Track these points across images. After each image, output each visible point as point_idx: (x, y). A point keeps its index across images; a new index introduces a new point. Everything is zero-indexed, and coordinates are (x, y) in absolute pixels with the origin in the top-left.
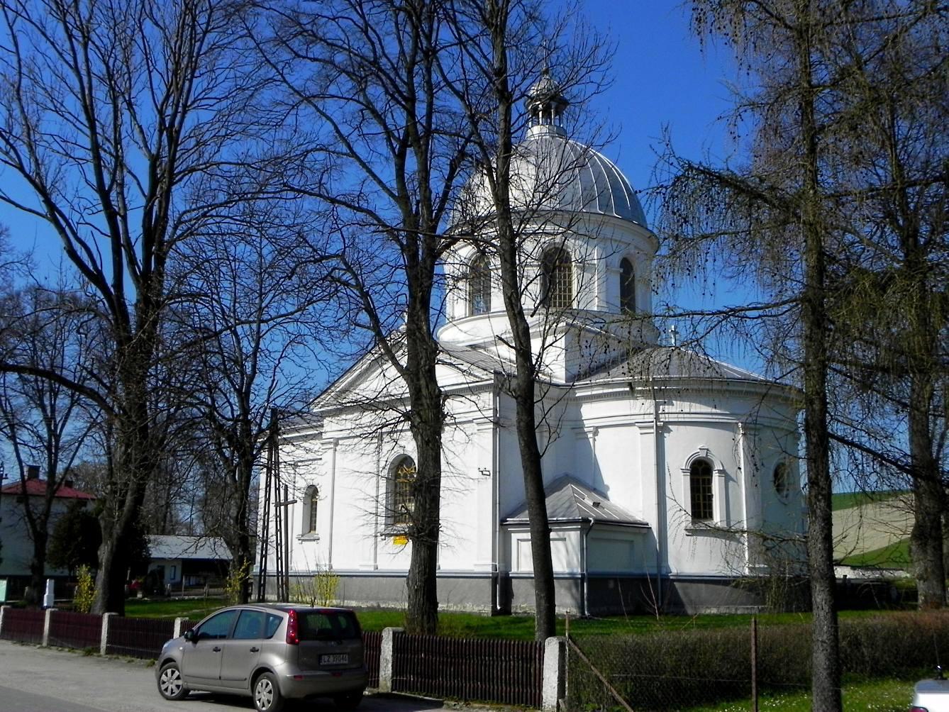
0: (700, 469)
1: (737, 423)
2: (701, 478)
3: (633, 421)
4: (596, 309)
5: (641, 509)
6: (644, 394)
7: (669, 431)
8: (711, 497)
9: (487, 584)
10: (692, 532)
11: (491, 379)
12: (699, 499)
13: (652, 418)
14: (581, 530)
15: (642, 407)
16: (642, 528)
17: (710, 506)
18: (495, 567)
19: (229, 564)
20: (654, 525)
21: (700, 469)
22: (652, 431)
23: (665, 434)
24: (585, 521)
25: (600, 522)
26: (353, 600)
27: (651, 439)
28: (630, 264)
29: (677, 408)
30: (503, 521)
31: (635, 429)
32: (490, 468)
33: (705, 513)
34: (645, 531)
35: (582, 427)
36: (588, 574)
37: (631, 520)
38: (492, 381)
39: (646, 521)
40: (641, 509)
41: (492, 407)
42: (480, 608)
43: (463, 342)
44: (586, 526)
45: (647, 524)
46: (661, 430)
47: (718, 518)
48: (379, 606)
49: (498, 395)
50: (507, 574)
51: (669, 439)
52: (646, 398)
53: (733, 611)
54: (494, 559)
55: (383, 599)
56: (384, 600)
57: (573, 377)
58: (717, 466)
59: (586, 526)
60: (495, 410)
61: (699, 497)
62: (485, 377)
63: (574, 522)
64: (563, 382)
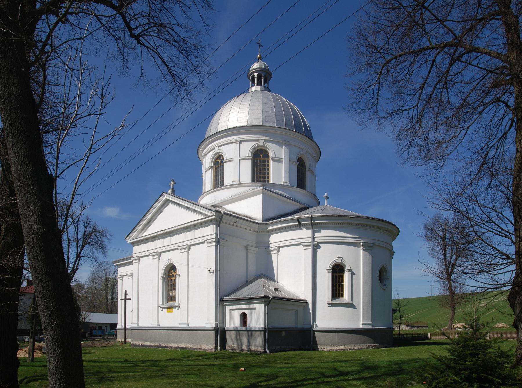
0: (338, 269)
1: (360, 243)
2: (338, 275)
3: (299, 242)
4: (283, 184)
5: (303, 293)
6: (306, 226)
7: (320, 247)
8: (343, 286)
9: (213, 333)
10: (331, 305)
11: (213, 215)
12: (336, 287)
13: (311, 240)
14: (264, 303)
15: (306, 234)
16: (304, 303)
17: (343, 291)
18: (216, 324)
19: (246, 326)
20: (310, 301)
21: (338, 269)
22: (310, 247)
23: (317, 249)
24: (267, 297)
25: (276, 298)
26: (148, 342)
27: (310, 252)
28: (303, 161)
29: (325, 234)
30: (221, 300)
31: (301, 247)
32: (214, 268)
33: (339, 294)
34: (305, 304)
35: (269, 247)
36: (269, 328)
37: (297, 298)
38: (214, 217)
39: (306, 299)
40: (303, 293)
41: (215, 232)
42: (209, 347)
43: (209, 204)
44: (267, 300)
45: (306, 301)
46: (316, 247)
47: (346, 297)
48: (160, 345)
49: (219, 226)
50: (224, 328)
51: (319, 252)
52: (307, 229)
53: (352, 348)
54: (216, 320)
55: (162, 342)
56: (163, 342)
57: (267, 219)
58: (347, 268)
59: (267, 300)
60: (217, 234)
61: (336, 285)
62: (211, 215)
63: (260, 298)
64: (261, 222)
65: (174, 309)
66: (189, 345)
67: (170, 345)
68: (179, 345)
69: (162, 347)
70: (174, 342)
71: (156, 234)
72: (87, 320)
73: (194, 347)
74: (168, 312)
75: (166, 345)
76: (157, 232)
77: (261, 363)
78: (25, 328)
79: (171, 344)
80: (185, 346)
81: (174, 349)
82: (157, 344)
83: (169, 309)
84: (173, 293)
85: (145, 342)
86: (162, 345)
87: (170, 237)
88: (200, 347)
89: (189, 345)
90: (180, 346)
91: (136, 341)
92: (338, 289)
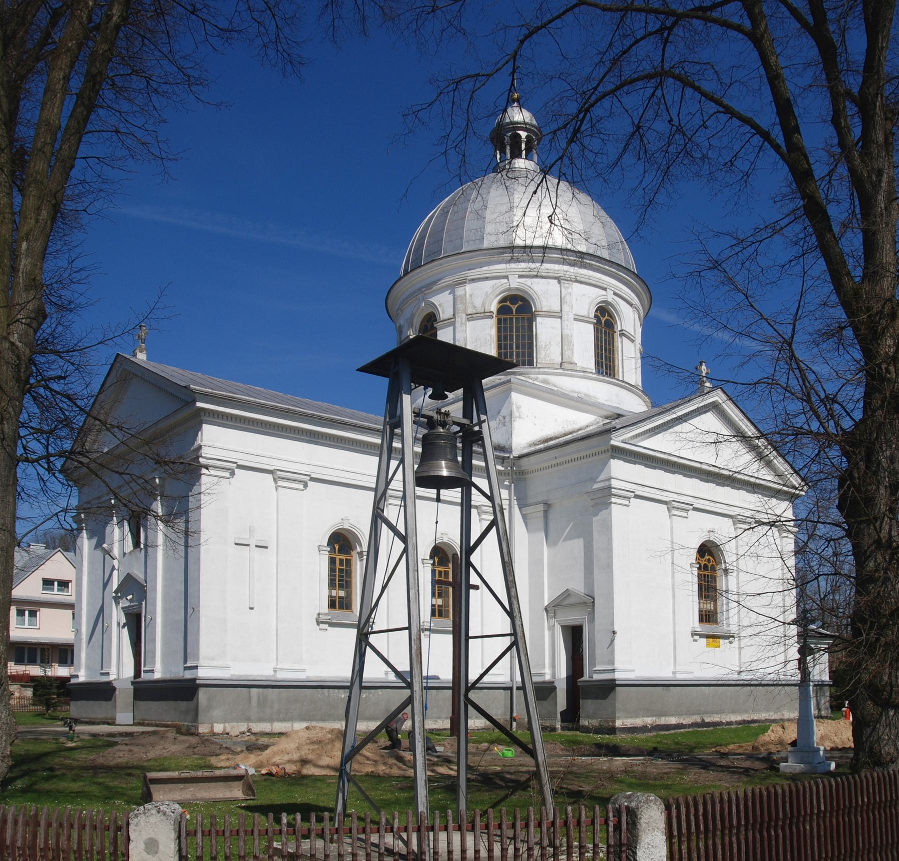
48: (703, 720)
55: (706, 713)
65: (721, 641)
66: (764, 715)
67: (725, 718)
68: (746, 717)
69: (709, 725)
70: (733, 712)
71: (698, 465)
72: (12, 608)
73: (773, 718)
74: (708, 645)
75: (718, 720)
76: (701, 463)
77: (654, 752)
78: (180, 702)
79: (728, 717)
80: (755, 718)
81: (734, 727)
82: (697, 719)
83: (711, 640)
84: (709, 605)
85: (663, 718)
86: (707, 720)
87: (714, 485)
88: (781, 717)
89: (764, 715)
90: (746, 719)
91: (631, 717)
92: (515, 353)
